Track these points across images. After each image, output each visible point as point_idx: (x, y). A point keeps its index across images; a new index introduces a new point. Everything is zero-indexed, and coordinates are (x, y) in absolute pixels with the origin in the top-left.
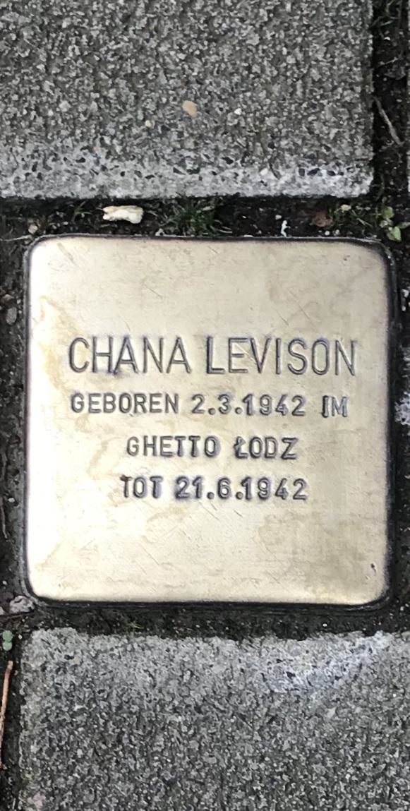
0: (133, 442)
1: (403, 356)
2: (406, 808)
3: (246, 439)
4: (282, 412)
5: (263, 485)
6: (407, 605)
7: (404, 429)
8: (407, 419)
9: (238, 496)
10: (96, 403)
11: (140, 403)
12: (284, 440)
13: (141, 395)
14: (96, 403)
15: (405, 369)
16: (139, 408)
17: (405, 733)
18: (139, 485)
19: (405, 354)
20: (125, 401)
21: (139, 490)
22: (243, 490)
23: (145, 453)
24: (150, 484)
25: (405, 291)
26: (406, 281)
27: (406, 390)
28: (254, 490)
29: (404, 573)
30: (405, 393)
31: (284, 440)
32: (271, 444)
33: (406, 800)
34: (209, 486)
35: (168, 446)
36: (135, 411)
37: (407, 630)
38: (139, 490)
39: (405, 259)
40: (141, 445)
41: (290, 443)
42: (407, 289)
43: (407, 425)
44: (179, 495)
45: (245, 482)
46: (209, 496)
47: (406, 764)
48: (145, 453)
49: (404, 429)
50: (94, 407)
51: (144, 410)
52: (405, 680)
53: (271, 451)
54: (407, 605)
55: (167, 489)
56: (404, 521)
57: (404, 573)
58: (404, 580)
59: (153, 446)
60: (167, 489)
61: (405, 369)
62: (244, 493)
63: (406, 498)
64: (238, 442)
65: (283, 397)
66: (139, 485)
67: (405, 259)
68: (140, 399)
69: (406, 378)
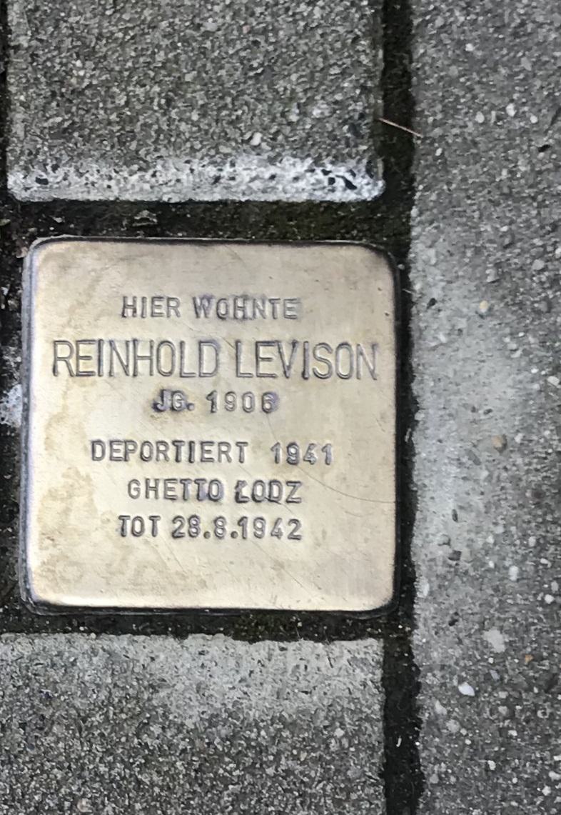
0: (134, 486)
1: (2, 355)
2: (5, 812)
3: (250, 481)
4: (310, 461)
5: (259, 525)
6: (6, 607)
7: (4, 429)
8: (7, 419)
9: (233, 535)
10: (118, 451)
11: (224, 452)
12: (288, 483)
13: (163, 443)
14: (118, 451)
15: (4, 368)
16: (161, 456)
17: (4, 736)
18: (138, 524)
19: (4, 352)
20: (146, 449)
21: (137, 529)
22: (239, 530)
23: (147, 497)
24: (148, 524)
25: (4, 289)
26: (5, 279)
27: (5, 389)
28: (250, 530)
29: (3, 574)
30: (5, 392)
31: (288, 483)
32: (275, 488)
33: (5, 804)
34: (205, 525)
35: (171, 489)
36: (157, 460)
37: (6, 632)
38: (137, 529)
39: (4, 256)
40: (143, 487)
41: (294, 486)
42: (6, 287)
43: (6, 425)
44: (176, 535)
45: (242, 521)
46: (206, 535)
47: (5, 767)
48: (147, 497)
49: (4, 429)
50: (115, 455)
51: (166, 458)
52: (4, 682)
53: (275, 494)
54: (6, 607)
55: (164, 527)
56: (3, 522)
57: (3, 574)
58: (3, 581)
59: (155, 489)
60: (164, 527)
61: (4, 368)
62: (240, 533)
63: (5, 498)
64: (240, 484)
65: (311, 446)
66: (138, 524)
67: (4, 256)
68: (162, 448)
69: (5, 377)
